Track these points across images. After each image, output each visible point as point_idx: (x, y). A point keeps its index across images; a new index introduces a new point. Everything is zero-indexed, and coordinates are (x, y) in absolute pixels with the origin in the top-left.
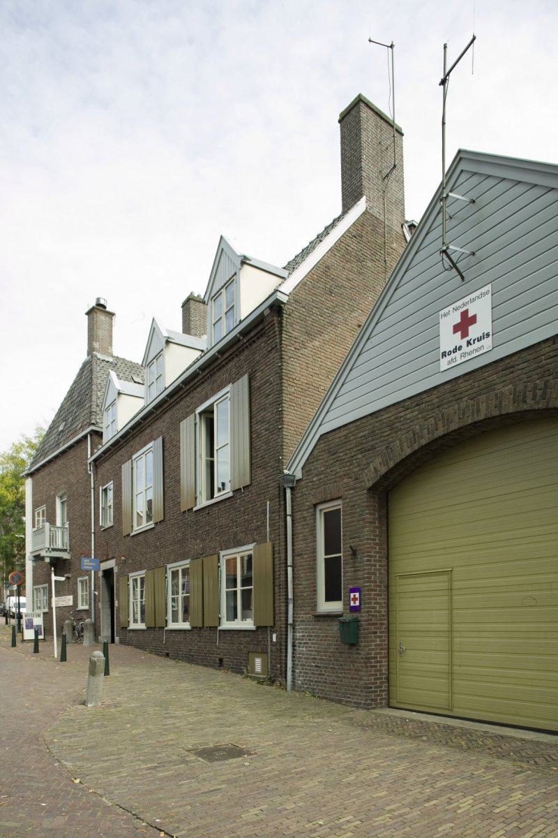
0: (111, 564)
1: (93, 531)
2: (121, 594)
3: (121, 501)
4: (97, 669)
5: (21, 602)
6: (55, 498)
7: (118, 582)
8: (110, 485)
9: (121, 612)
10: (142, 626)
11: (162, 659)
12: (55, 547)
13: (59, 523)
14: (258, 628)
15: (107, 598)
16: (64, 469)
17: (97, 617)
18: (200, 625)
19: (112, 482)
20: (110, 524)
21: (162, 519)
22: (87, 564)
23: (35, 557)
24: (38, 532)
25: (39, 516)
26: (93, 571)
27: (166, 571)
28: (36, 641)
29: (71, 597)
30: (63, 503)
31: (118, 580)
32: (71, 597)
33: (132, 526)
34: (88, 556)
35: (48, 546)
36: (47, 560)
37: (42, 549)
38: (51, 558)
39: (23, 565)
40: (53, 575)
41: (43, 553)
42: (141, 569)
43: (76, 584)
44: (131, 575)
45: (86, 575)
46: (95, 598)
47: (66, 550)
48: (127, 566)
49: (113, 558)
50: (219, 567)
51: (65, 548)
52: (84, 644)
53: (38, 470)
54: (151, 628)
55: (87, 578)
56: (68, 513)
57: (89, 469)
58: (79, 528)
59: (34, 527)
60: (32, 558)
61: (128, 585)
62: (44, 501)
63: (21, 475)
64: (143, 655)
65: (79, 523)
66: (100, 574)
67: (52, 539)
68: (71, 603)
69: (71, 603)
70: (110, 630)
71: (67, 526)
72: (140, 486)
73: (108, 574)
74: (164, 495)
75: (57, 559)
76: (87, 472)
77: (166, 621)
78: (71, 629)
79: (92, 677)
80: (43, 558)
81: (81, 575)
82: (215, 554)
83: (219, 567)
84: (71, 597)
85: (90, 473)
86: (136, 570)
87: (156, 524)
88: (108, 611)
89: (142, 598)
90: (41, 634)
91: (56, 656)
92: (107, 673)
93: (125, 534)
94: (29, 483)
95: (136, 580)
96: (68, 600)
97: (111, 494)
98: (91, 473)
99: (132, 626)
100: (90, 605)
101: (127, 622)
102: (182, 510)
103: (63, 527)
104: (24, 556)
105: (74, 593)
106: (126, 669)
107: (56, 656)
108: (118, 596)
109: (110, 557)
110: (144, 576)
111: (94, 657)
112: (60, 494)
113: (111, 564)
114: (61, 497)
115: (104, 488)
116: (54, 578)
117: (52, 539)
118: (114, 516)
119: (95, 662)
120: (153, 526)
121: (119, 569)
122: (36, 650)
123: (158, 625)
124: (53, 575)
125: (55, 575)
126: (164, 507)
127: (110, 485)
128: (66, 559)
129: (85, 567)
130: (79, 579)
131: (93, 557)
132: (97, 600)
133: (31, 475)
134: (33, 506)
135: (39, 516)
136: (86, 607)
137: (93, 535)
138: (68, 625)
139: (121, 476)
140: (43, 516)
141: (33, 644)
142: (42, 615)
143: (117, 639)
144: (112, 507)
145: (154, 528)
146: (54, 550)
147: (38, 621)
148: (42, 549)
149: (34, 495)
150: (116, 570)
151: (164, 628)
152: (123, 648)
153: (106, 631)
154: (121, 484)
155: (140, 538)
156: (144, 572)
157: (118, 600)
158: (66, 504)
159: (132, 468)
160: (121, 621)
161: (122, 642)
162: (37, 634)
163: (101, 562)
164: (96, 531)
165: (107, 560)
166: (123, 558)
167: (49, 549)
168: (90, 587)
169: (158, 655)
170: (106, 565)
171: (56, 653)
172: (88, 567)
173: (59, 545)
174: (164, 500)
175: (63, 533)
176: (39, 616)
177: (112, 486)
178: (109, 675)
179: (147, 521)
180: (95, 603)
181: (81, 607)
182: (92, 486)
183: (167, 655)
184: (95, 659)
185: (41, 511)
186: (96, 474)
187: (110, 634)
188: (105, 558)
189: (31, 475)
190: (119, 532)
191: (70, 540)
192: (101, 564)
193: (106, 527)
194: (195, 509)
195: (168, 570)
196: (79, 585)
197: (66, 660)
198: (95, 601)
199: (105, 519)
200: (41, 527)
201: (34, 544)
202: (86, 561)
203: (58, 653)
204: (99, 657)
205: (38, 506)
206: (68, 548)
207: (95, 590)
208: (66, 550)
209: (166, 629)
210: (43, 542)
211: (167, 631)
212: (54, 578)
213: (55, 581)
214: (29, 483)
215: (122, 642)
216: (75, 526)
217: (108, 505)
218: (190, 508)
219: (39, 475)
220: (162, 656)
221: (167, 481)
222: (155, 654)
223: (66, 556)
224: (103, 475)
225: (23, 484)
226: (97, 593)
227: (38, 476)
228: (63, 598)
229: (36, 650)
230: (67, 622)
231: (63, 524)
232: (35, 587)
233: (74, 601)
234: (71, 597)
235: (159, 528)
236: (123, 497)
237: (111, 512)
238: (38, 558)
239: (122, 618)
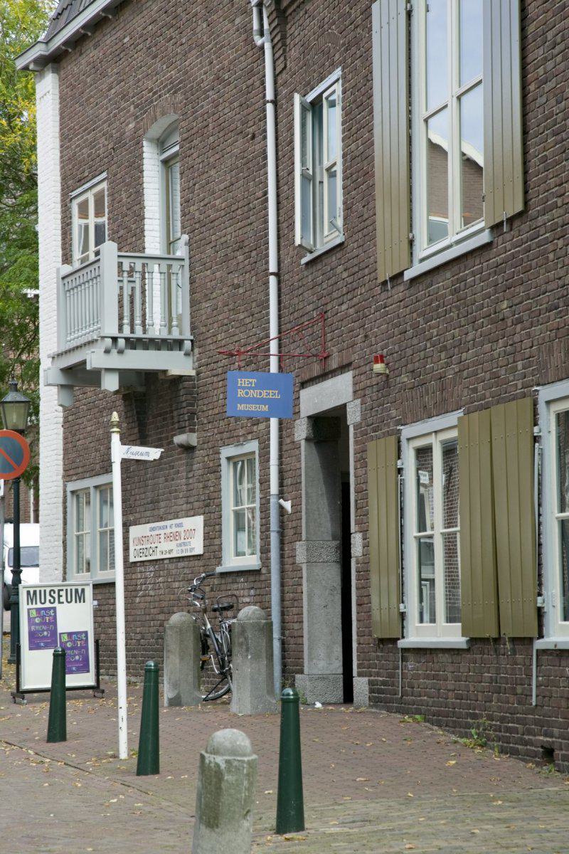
0: (335, 392)
1: (273, 267)
2: (373, 501)
3: (370, 144)
4: (225, 799)
5: (23, 543)
6: (139, 144)
7: (362, 462)
8: (332, 85)
9: (374, 578)
10: (450, 635)
11: (526, 771)
12: (139, 333)
13: (153, 242)
14: (472, 641)
15: (327, 526)
16: (169, 33)
17: (290, 603)
18: (495, 635)
19: (338, 73)
20: (330, 236)
21: (519, 207)
22: (247, 393)
23: (68, 371)
24: (79, 277)
25: (84, 213)
26: (274, 423)
27: (535, 413)
28: (58, 694)
29: (197, 522)
30: (166, 162)
31: (362, 452)
32: (196, 523)
33: (411, 243)
34: (256, 361)
35: (115, 333)
36: (111, 383)
37: (90, 343)
38: (123, 374)
39: (32, 406)
40: (116, 438)
41: (95, 359)
42: (442, 409)
43: (216, 470)
44: (407, 431)
45: (249, 435)
46: (282, 525)
47: (178, 344)
48: (396, 398)
49: (343, 368)
50: (536, 439)
51: (176, 334)
52: (234, 707)
53: (78, 41)
54: (484, 640)
55: (253, 446)
56: (186, 202)
57: (256, 26)
58: (226, 259)
59: (67, 259)
60: (61, 380)
61: (400, 471)
62: (100, 159)
63: (20, 64)
64: (455, 753)
65: (224, 238)
66: (301, 431)
67: (131, 305)
68: (197, 547)
69: (197, 547)
70: (338, 650)
71: (181, 251)
72: (439, 80)
73: (328, 428)
74: (524, 115)
75: (150, 377)
76: (249, 41)
77: (540, 613)
78: (191, 644)
79: (204, 830)
80: (94, 377)
81: (235, 439)
82: (524, 396)
83: (536, 439)
84: (197, 522)
85: (259, 41)
86: (428, 413)
87: (496, 228)
88: (332, 575)
89: (449, 522)
90: (85, 669)
91: (123, 754)
92: (290, 815)
93: (384, 273)
94: (48, 88)
95: (423, 454)
96: (181, 536)
97: (333, 119)
98: (265, 42)
99: (418, 635)
100: (265, 551)
101: (396, 616)
102: (381, 280)
103: (168, 259)
104: (32, 371)
105: (210, 508)
106: (374, 808)
107: (123, 754)
108: (364, 515)
109: (334, 364)
110: (454, 434)
111: (216, 752)
112: (156, 130)
113: (335, 392)
114: (161, 143)
115: (311, 97)
116: (119, 451)
117: (131, 305)
118: (348, 208)
119: (218, 774)
120: (485, 238)
121: (367, 411)
122: (57, 731)
123: (508, 632)
124: (116, 438)
125: (124, 441)
126: (525, 163)
127: (332, 85)
128: (179, 379)
129: (241, 407)
130: (227, 452)
131: (274, 368)
132: (289, 533)
133: (54, 61)
134: (64, 179)
135: (84, 213)
136: (251, 561)
137: (273, 281)
138: (180, 630)
139: (369, 49)
140: (99, 213)
141: (46, 706)
142: (89, 592)
143: (361, 685)
144: (339, 169)
145: (486, 247)
146: (133, 344)
147: (75, 618)
148: (90, 343)
149: (66, 137)
150: (354, 416)
151: (531, 640)
152: (386, 724)
153: (321, 652)
154: (368, 78)
155: (442, 284)
156: (452, 418)
157: (364, 532)
158: (177, 168)
159: (409, 14)
160: (376, 614)
161: (380, 698)
162: (61, 666)
163: (304, 385)
164: (284, 269)
165: (324, 376)
166: (379, 367)
167: (115, 339)
168: (265, 481)
169: (514, 753)
170: (317, 399)
171: (125, 746)
172: (253, 408)
173: (157, 330)
174: (525, 132)
175: (168, 276)
176: (80, 596)
177: (338, 88)
178: (300, 827)
179: (467, 221)
180: (282, 542)
181: (231, 562)
182: (269, 95)
183: (549, 753)
184: (220, 760)
185: (90, 196)
186: (281, 45)
187: (337, 666)
188: (316, 369)
189: (54, 61)
190: (366, 267)
191: (194, 303)
192: (304, 394)
193: (321, 249)
194: (408, 275)
195: (542, 407)
196: (227, 476)
197: (156, 770)
198: (282, 535)
199: (312, 219)
200: (92, 258)
201: (66, 324)
202: (243, 382)
203: (130, 740)
204: (234, 752)
205: (81, 181)
206: (187, 335)
207: (281, 495)
208: (178, 344)
209: (539, 644)
210: (97, 317)
211: (542, 652)
212: (119, 451)
213: (126, 463)
214: (48, 88)
215: (380, 698)
216: (209, 251)
217: (326, 164)
218: (396, 271)
219: (83, 60)
220: (526, 757)
221: (537, 54)
222: (503, 751)
223: (178, 364)
224: (306, 48)
225: (30, 96)
226: (288, 505)
227: (79, 65)
228: (170, 525)
229: (57, 731)
230: (176, 618)
231: (170, 244)
232: (72, 486)
233: (207, 537)
234: (196, 523)
235: (507, 243)
236: (377, 131)
237: (334, 195)
238: (78, 377)
239: (379, 604)
